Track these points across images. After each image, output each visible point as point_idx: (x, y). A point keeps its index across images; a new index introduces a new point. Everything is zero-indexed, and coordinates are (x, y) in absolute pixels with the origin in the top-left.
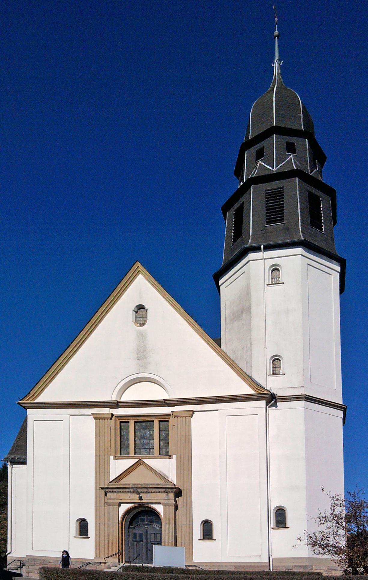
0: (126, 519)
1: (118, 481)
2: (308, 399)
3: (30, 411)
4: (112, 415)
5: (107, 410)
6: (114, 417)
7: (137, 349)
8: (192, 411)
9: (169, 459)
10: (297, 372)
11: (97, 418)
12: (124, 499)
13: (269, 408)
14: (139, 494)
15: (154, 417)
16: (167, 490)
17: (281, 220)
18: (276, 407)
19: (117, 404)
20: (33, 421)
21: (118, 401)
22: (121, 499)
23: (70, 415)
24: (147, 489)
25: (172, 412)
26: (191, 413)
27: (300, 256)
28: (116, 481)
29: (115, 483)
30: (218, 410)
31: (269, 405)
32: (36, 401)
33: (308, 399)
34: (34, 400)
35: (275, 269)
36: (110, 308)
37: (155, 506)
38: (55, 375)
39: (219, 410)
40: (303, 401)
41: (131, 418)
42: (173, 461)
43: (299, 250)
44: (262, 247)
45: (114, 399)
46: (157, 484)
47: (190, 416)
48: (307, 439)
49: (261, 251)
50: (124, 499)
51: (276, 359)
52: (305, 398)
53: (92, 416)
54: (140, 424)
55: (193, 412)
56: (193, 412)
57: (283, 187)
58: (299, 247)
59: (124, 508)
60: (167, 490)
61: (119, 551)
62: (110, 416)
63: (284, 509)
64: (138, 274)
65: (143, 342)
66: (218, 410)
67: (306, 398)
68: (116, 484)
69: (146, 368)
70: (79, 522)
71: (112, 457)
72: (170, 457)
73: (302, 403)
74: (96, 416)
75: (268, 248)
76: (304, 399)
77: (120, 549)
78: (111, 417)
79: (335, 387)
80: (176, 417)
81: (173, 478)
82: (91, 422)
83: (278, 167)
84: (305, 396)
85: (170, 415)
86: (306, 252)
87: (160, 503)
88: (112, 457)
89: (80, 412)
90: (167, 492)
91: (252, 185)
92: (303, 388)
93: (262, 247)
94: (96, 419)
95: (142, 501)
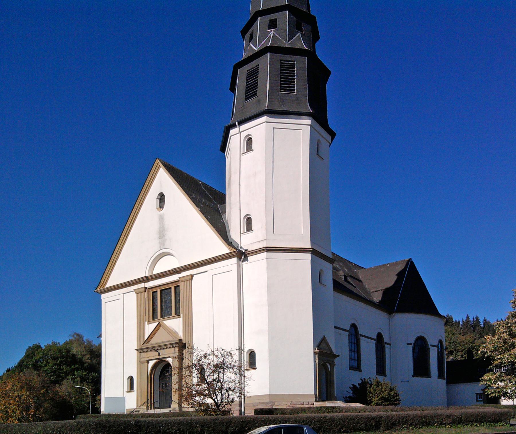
0: (154, 373)
1: (148, 342)
2: (269, 250)
3: (103, 296)
4: (146, 288)
5: (142, 285)
6: (147, 290)
7: (159, 230)
8: (191, 275)
9: (179, 318)
10: (262, 227)
11: (138, 292)
12: (150, 357)
13: (243, 263)
14: (156, 351)
15: (171, 285)
16: (173, 345)
17: (286, 90)
18: (247, 261)
19: (146, 279)
20: (104, 303)
21: (146, 277)
22: (148, 357)
23: (124, 294)
24: (161, 346)
25: (179, 278)
26: (190, 277)
27: (265, 123)
28: (147, 342)
29: (147, 344)
30: (206, 271)
31: (242, 260)
32: (106, 287)
33: (269, 250)
34: (105, 287)
35: (249, 141)
36: (142, 203)
37: (167, 359)
38: (114, 264)
39: (208, 271)
40: (266, 253)
41: (158, 288)
42: (181, 319)
43: (264, 118)
44: (237, 123)
45: (150, 275)
46: (169, 341)
47: (189, 280)
48: (270, 287)
49: (237, 127)
50: (150, 357)
51: (249, 221)
52: (266, 250)
53: (134, 292)
54: (165, 292)
55: (192, 276)
56: (192, 276)
57: (258, 65)
58: (264, 116)
59: (151, 363)
60: (173, 345)
61: (148, 400)
62: (144, 289)
63: (253, 351)
64: (159, 168)
65: (162, 224)
66: (206, 271)
67: (266, 250)
68: (148, 344)
69: (164, 245)
70: (129, 379)
71: (146, 322)
72: (179, 317)
73: (264, 255)
74: (137, 291)
75: (241, 123)
76: (265, 251)
77: (149, 398)
78: (145, 290)
79: (302, 233)
80: (182, 282)
81: (181, 335)
82: (134, 295)
83: (260, 46)
84: (265, 248)
85: (179, 281)
86: (271, 118)
87: (169, 357)
88: (146, 322)
89: (128, 290)
90: (174, 347)
91: (239, 69)
92: (265, 241)
93: (237, 123)
94: (137, 293)
95: (161, 357)
